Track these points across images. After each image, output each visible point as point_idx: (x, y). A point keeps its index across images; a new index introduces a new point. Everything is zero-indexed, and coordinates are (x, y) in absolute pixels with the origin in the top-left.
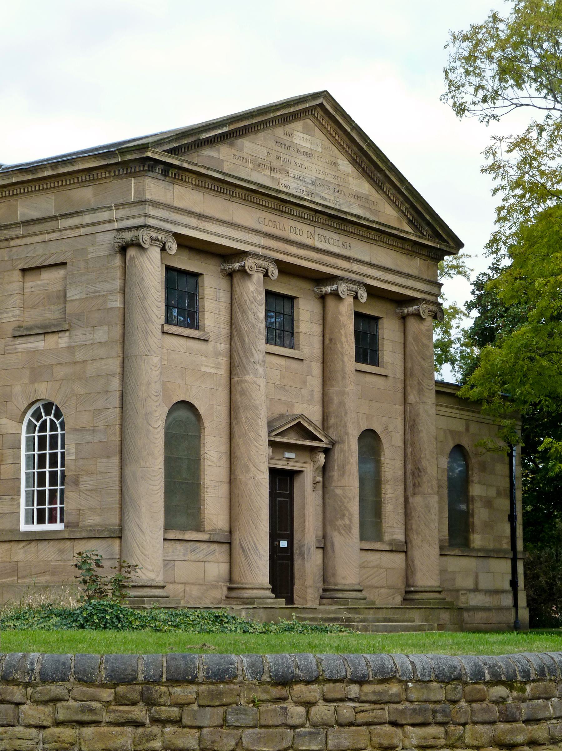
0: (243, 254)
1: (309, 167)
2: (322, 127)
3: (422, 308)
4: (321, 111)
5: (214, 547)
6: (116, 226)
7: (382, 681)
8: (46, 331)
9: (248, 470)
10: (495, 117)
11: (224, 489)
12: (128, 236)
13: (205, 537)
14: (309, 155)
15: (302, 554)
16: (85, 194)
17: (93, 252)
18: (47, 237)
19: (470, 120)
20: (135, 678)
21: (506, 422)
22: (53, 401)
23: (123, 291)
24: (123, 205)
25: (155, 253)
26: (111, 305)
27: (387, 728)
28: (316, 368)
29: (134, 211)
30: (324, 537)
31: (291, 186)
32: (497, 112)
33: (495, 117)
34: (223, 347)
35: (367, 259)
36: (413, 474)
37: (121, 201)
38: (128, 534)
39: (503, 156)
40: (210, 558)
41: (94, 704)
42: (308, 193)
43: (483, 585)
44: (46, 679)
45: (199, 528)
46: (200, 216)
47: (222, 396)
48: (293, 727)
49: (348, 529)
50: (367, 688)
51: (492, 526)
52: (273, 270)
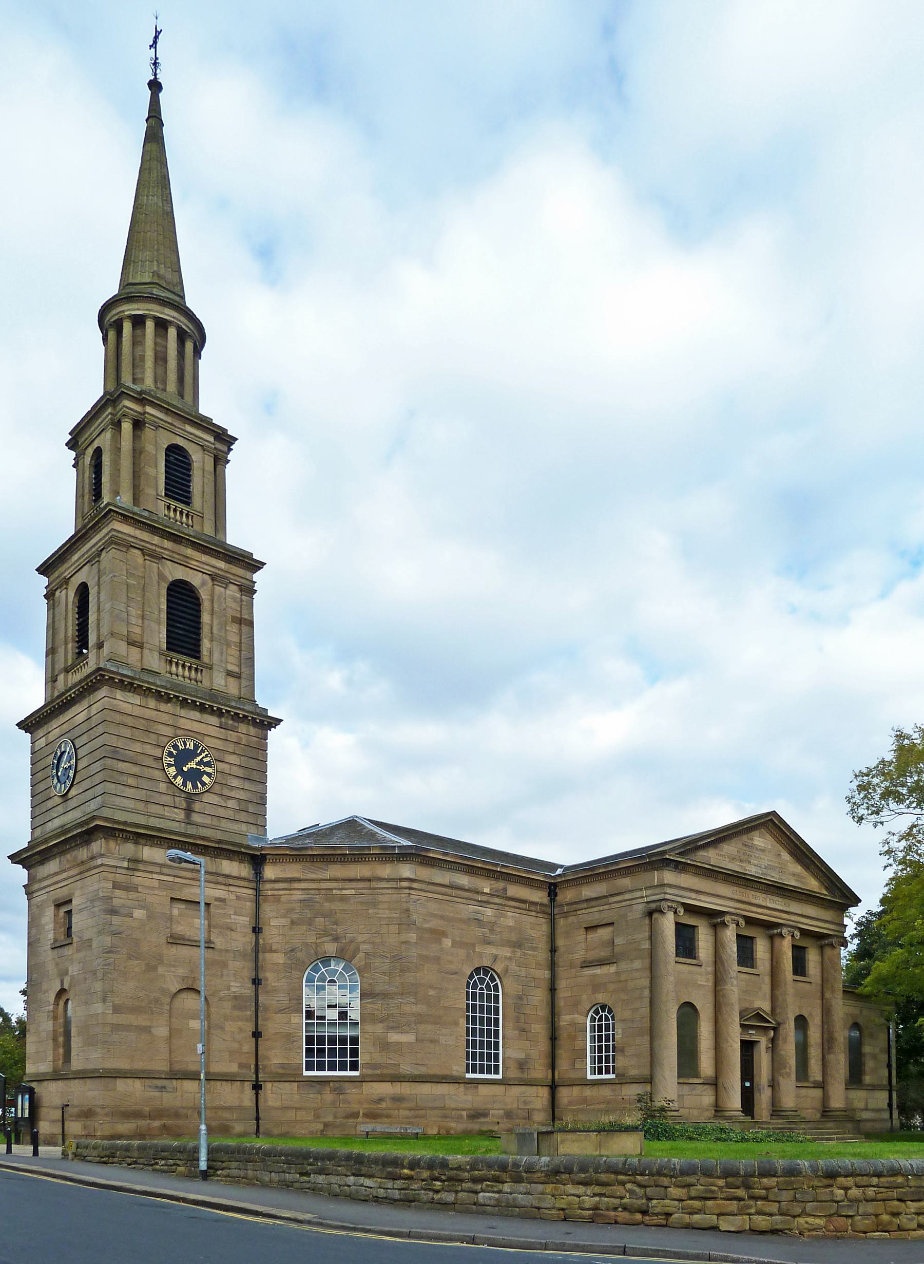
0: (723, 913)
1: (764, 858)
2: (771, 834)
3: (834, 940)
4: (771, 823)
5: (706, 1087)
6: (645, 900)
7: (891, 1176)
8: (601, 963)
9: (727, 1041)
10: (882, 823)
11: (711, 1054)
12: (653, 906)
13: (701, 1081)
14: (763, 851)
15: (759, 1090)
16: (625, 882)
17: (631, 916)
18: (601, 908)
19: (867, 825)
20: (739, 1173)
21: (888, 1008)
22: (606, 1003)
23: (651, 938)
24: (650, 887)
25: (670, 916)
26: (643, 947)
27: (896, 1203)
28: (767, 980)
29: (657, 891)
30: (773, 1080)
31: (752, 870)
32: (882, 819)
33: (882, 823)
34: (710, 969)
35: (800, 912)
36: (828, 1041)
37: (649, 885)
38: (656, 1080)
39: (894, 844)
40: (704, 1093)
41: (713, 1188)
42: (763, 874)
43: (870, 1106)
44: (684, 1173)
45: (697, 1076)
46: (697, 892)
47: (710, 998)
48: (837, 1202)
49: (789, 1075)
50: (882, 1179)
51: (876, 1069)
52: (742, 922)
